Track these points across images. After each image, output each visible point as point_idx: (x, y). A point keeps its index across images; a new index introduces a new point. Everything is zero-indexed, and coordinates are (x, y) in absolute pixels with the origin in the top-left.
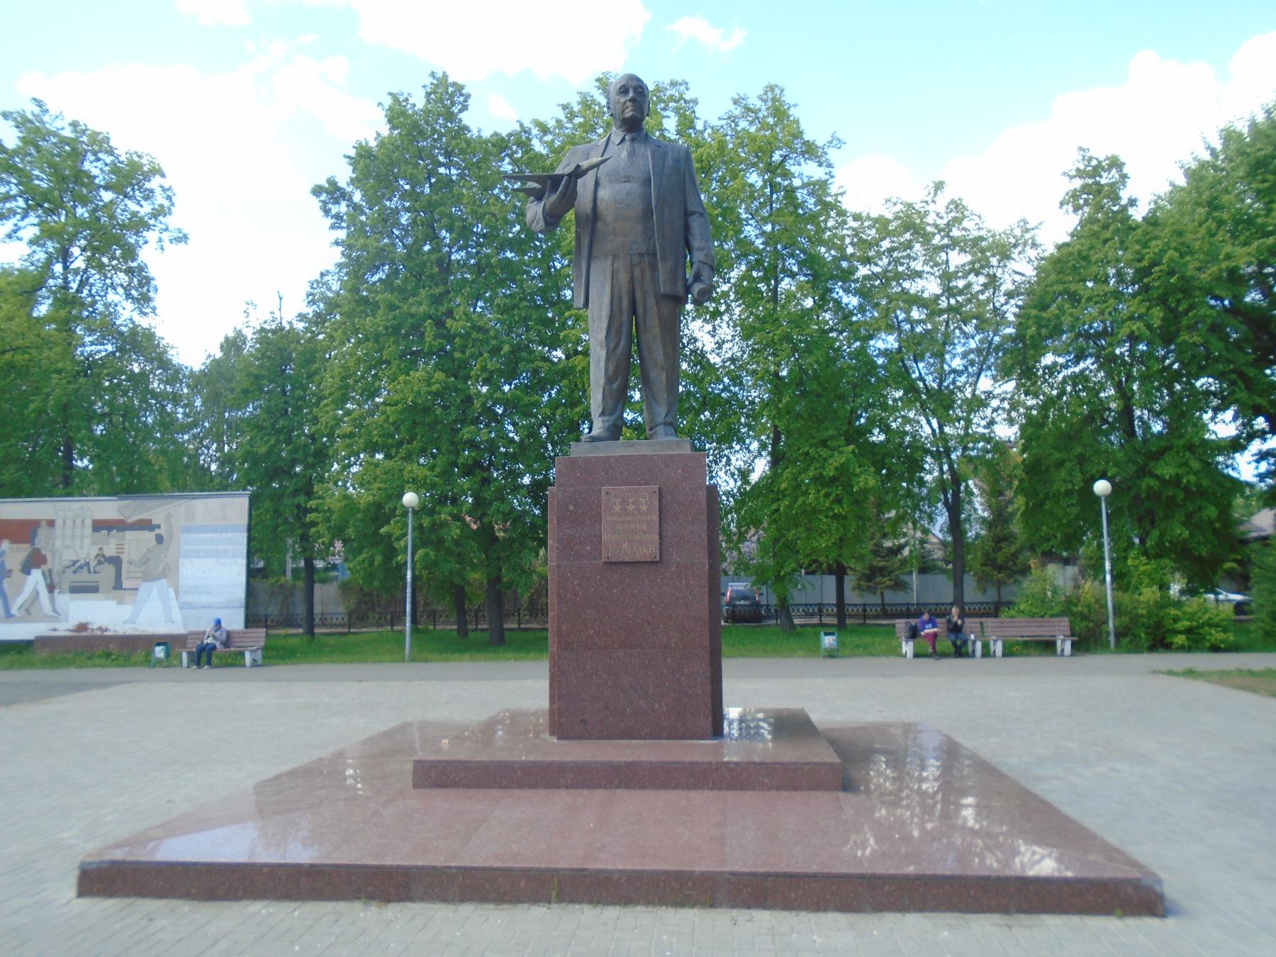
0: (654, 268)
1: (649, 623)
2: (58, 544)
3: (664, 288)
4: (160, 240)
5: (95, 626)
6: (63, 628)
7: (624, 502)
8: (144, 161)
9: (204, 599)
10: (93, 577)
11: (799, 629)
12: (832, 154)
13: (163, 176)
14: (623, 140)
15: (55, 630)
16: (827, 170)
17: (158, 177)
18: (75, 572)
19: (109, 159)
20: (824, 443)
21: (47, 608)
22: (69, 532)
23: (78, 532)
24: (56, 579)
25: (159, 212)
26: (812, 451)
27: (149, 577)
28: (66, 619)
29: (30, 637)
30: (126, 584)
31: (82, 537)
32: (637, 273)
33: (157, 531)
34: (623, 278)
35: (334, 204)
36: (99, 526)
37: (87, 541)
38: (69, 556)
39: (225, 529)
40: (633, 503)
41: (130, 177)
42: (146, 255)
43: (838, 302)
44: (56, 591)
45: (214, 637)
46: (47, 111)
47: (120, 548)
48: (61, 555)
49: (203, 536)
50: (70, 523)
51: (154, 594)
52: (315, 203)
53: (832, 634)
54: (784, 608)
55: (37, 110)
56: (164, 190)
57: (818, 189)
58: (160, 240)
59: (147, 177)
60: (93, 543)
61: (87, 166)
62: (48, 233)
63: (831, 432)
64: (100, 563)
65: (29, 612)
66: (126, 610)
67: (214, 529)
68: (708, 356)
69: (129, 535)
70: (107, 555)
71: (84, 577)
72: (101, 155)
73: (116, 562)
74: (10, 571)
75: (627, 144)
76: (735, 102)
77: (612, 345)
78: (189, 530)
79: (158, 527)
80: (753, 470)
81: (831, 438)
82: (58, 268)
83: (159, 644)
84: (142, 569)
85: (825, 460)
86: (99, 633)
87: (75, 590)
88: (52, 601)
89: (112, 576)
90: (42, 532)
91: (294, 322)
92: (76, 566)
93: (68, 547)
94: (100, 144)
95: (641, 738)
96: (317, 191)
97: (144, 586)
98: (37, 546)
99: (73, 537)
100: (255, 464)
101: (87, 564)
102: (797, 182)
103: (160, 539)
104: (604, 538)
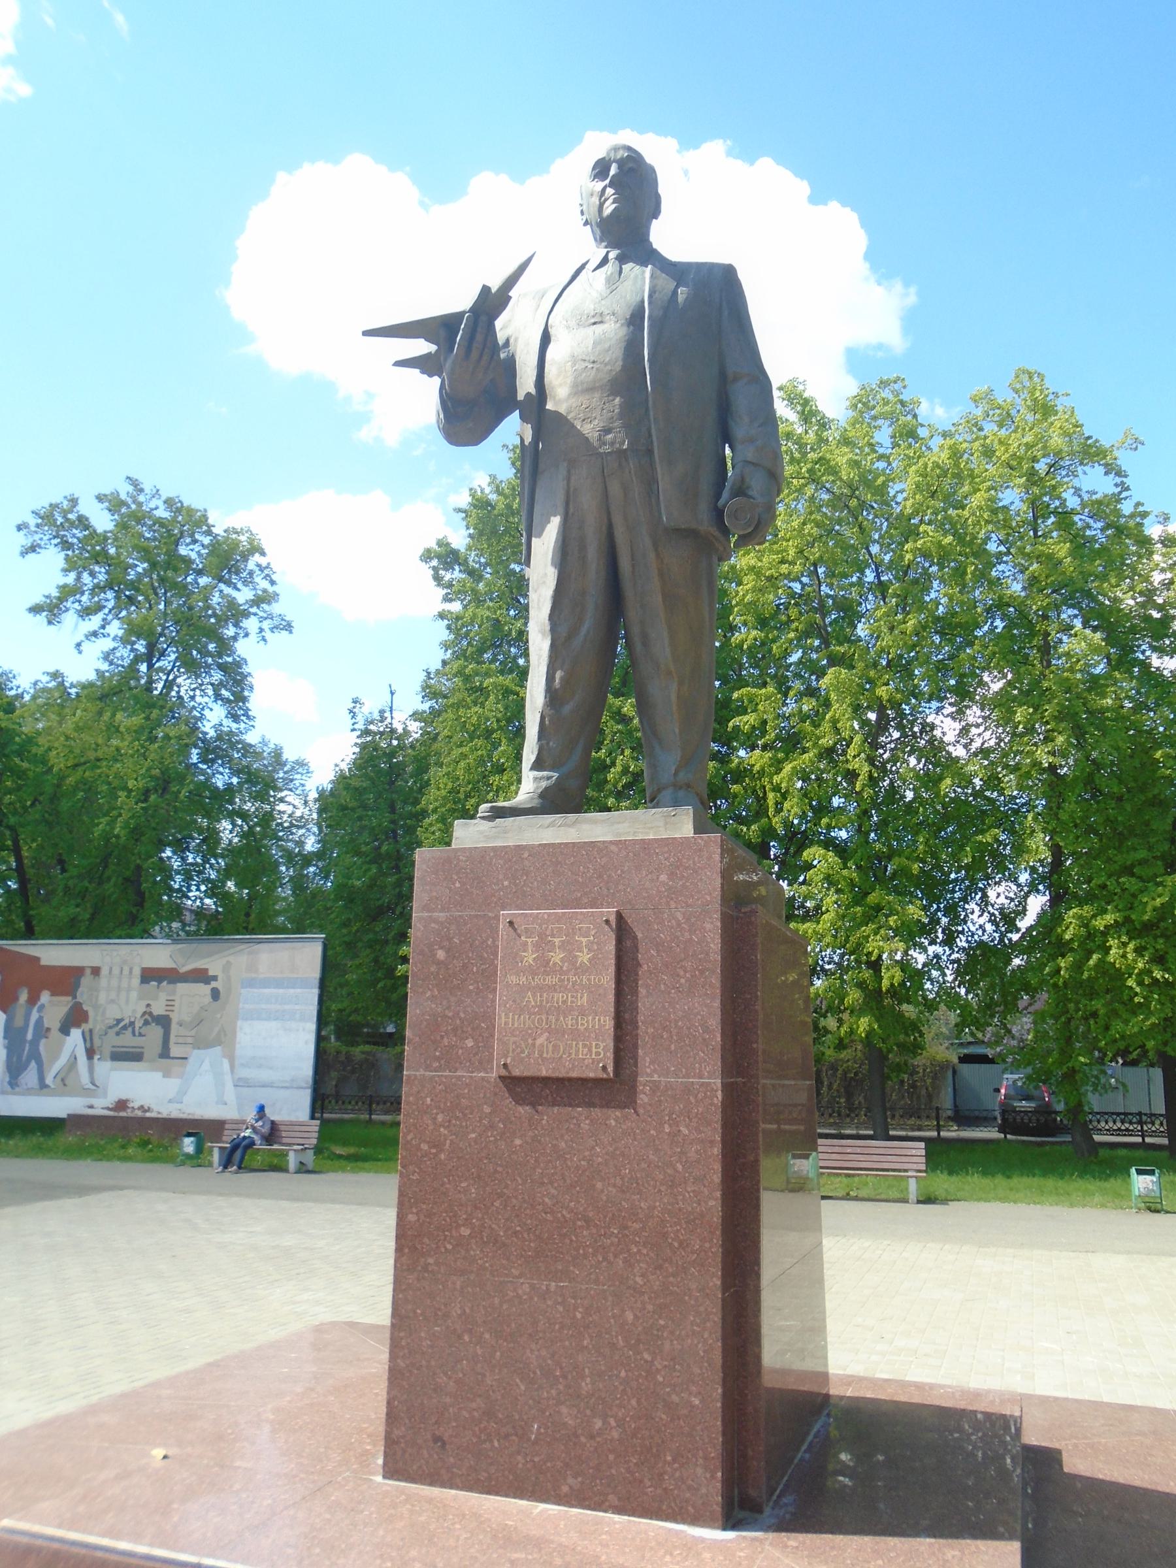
0: (650, 484)
1: (587, 1221)
2: (102, 997)
3: (671, 512)
4: (261, 630)
5: (136, 1105)
6: (100, 1106)
7: (543, 943)
8: (243, 538)
9: (264, 1075)
10: (137, 1041)
11: (1103, 1153)
12: (1124, 459)
13: (263, 554)
14: (604, 261)
15: (91, 1107)
16: (1118, 480)
17: (257, 555)
18: (118, 1034)
19: (206, 540)
20: (1128, 871)
21: (85, 1079)
22: (114, 982)
23: (124, 984)
24: (97, 1042)
25: (262, 599)
26: (1111, 884)
27: (202, 1043)
28: (105, 1095)
29: (63, 1115)
30: (175, 1051)
31: (129, 990)
32: (615, 489)
33: (214, 984)
34: (588, 502)
35: (446, 570)
36: (150, 976)
37: (134, 995)
38: (113, 1013)
39: (292, 983)
40: (562, 946)
41: (229, 558)
42: (244, 648)
43: (1145, 665)
44: (96, 1057)
45: (254, 1129)
46: (142, 490)
47: (170, 1004)
48: (104, 1013)
49: (266, 991)
50: (116, 971)
51: (206, 1065)
52: (426, 571)
53: (1152, 1173)
54: (1079, 1121)
55: (131, 489)
56: (262, 569)
57: (1102, 508)
58: (261, 630)
59: (245, 557)
60: (140, 998)
61: (183, 551)
62: (133, 631)
63: (1142, 854)
64: (146, 1023)
65: (65, 1083)
66: (172, 1085)
67: (279, 983)
68: (951, 748)
69: (182, 987)
70: (155, 1013)
71: (127, 1040)
72: (197, 536)
73: (164, 1022)
74: (48, 1029)
75: (609, 268)
76: (975, 400)
77: (563, 630)
78: (250, 984)
79: (215, 978)
80: (1025, 910)
81: (1142, 862)
82: (143, 668)
83: (189, 1135)
84: (193, 1033)
85: (1134, 896)
86: (139, 1113)
87: (119, 1056)
88: (91, 1070)
89: (153, 1041)
90: (86, 980)
91: (408, 723)
92: (122, 1026)
93: (113, 1001)
94: (197, 521)
95: (560, 1500)
96: (427, 556)
97: (195, 1055)
98: (79, 999)
99: (119, 989)
100: (351, 900)
101: (132, 1024)
102: (1072, 502)
103: (215, 994)
104: (501, 1019)
